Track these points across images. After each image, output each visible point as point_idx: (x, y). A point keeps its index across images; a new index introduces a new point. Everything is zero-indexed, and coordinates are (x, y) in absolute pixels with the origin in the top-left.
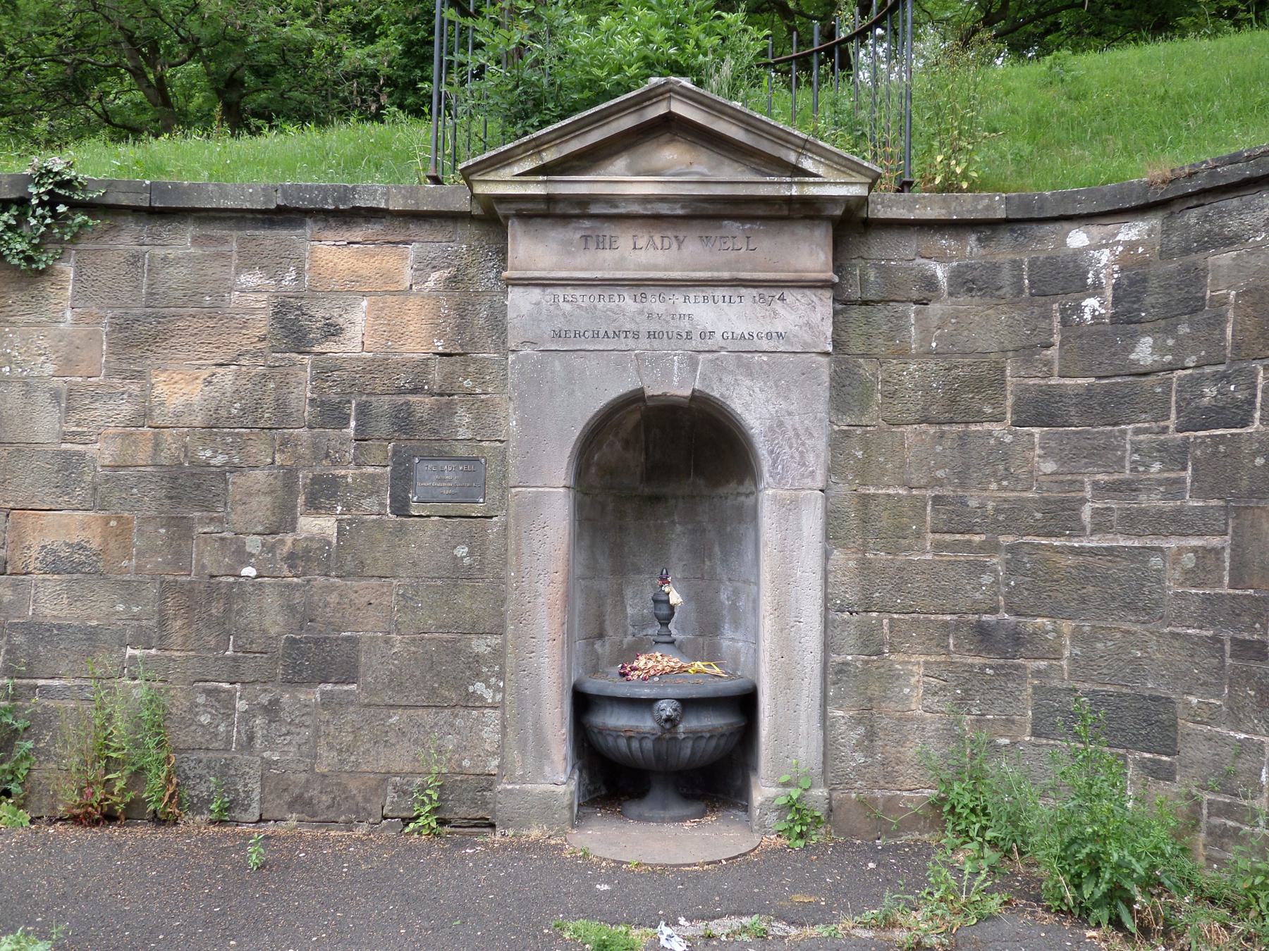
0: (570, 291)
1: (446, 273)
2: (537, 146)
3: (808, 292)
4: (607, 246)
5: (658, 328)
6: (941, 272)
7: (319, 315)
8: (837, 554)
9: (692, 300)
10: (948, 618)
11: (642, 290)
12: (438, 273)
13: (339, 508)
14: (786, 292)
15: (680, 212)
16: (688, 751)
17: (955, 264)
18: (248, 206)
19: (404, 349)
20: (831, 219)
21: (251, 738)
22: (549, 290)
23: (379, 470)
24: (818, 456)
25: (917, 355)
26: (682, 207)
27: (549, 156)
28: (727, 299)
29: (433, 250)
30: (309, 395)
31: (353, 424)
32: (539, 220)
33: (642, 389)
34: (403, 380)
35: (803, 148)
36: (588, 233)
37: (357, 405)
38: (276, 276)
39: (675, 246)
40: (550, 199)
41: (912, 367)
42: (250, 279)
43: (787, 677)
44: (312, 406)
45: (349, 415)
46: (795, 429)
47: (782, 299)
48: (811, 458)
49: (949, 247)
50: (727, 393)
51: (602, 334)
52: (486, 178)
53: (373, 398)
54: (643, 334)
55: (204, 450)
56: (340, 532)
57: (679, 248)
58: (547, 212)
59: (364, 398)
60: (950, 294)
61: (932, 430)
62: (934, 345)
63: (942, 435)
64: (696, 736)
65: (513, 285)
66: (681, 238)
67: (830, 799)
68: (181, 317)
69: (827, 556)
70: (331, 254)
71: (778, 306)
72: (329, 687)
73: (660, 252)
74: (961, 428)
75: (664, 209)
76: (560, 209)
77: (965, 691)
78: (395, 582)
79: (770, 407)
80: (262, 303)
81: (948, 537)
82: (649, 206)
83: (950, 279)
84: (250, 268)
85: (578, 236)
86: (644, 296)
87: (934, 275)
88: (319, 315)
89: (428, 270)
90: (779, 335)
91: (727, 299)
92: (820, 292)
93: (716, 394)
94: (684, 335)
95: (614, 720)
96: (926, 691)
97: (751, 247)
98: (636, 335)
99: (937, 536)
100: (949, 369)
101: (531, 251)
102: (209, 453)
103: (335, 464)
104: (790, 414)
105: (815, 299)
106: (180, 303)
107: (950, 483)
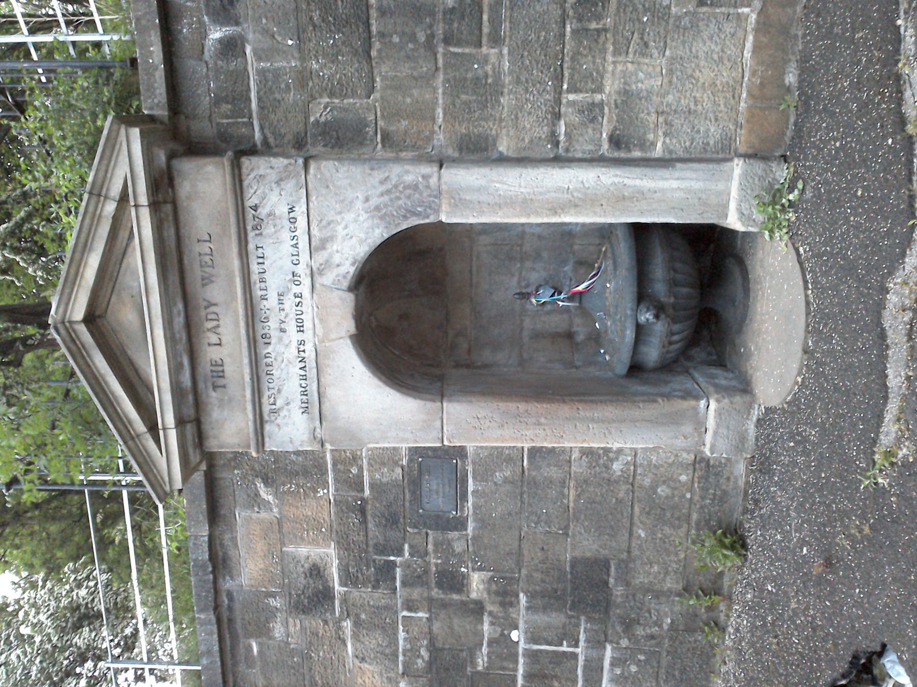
0: (265, 400)
1: (261, 486)
2: (133, 438)
3: (245, 183)
4: (221, 369)
5: (294, 323)
6: (216, 34)
7: (304, 582)
8: (503, 147)
9: (263, 293)
10: (568, 29)
11: (259, 338)
12: (262, 493)
13: (463, 569)
14: (248, 204)
15: (180, 306)
16: (685, 290)
17: (206, 18)
18: (215, 636)
19: (327, 519)
20: (171, 156)
21: (652, 637)
22: (266, 417)
23: (430, 539)
24: (407, 172)
25: (303, 59)
26: (175, 304)
27: (139, 426)
28: (261, 260)
29: (241, 496)
30: (369, 590)
31: (392, 558)
32: (203, 427)
33: (351, 337)
34: (354, 519)
35: (99, 195)
36: (210, 385)
37: (376, 554)
38: (272, 613)
39: (213, 309)
40: (180, 422)
41: (315, 66)
42: (278, 631)
43: (621, 199)
44: (379, 588)
45: (385, 561)
46: (382, 195)
47: (255, 208)
48: (409, 178)
49: (190, 25)
50: (351, 260)
51: (303, 373)
52: (166, 479)
53: (371, 543)
54: (301, 336)
55: (417, 664)
56: (480, 569)
57: (215, 305)
58: (194, 423)
59: (371, 549)
60: (237, 23)
61: (377, 45)
62: (290, 42)
63: (382, 35)
64: (673, 283)
65: (263, 445)
66: (205, 303)
67: (746, 156)
68: (312, 677)
69: (503, 160)
70: (250, 569)
71: (263, 212)
72: (612, 580)
73: (221, 322)
74: (374, 13)
75: (179, 321)
76: (190, 412)
77: (646, 10)
78: (525, 529)
79: (361, 218)
80: (295, 625)
81: (486, 30)
82: (178, 336)
83: (222, 24)
84: (269, 630)
85: (214, 394)
86: (264, 336)
87: (220, 41)
88: (304, 582)
89: (259, 500)
90: (291, 210)
91: (261, 260)
92: (244, 171)
93: (352, 270)
94: (298, 300)
95: (652, 354)
96: (643, 55)
97: (207, 238)
98: (302, 343)
99: (484, 40)
100: (315, 26)
101: (230, 429)
102: (420, 661)
103: (426, 572)
104: (367, 200)
105: (252, 176)
106: (301, 678)
107: (431, 26)
